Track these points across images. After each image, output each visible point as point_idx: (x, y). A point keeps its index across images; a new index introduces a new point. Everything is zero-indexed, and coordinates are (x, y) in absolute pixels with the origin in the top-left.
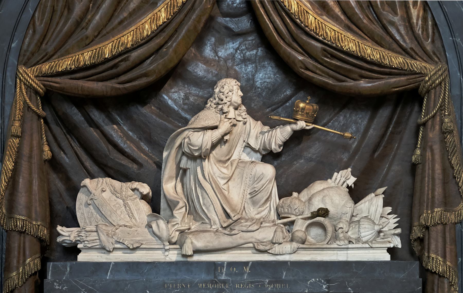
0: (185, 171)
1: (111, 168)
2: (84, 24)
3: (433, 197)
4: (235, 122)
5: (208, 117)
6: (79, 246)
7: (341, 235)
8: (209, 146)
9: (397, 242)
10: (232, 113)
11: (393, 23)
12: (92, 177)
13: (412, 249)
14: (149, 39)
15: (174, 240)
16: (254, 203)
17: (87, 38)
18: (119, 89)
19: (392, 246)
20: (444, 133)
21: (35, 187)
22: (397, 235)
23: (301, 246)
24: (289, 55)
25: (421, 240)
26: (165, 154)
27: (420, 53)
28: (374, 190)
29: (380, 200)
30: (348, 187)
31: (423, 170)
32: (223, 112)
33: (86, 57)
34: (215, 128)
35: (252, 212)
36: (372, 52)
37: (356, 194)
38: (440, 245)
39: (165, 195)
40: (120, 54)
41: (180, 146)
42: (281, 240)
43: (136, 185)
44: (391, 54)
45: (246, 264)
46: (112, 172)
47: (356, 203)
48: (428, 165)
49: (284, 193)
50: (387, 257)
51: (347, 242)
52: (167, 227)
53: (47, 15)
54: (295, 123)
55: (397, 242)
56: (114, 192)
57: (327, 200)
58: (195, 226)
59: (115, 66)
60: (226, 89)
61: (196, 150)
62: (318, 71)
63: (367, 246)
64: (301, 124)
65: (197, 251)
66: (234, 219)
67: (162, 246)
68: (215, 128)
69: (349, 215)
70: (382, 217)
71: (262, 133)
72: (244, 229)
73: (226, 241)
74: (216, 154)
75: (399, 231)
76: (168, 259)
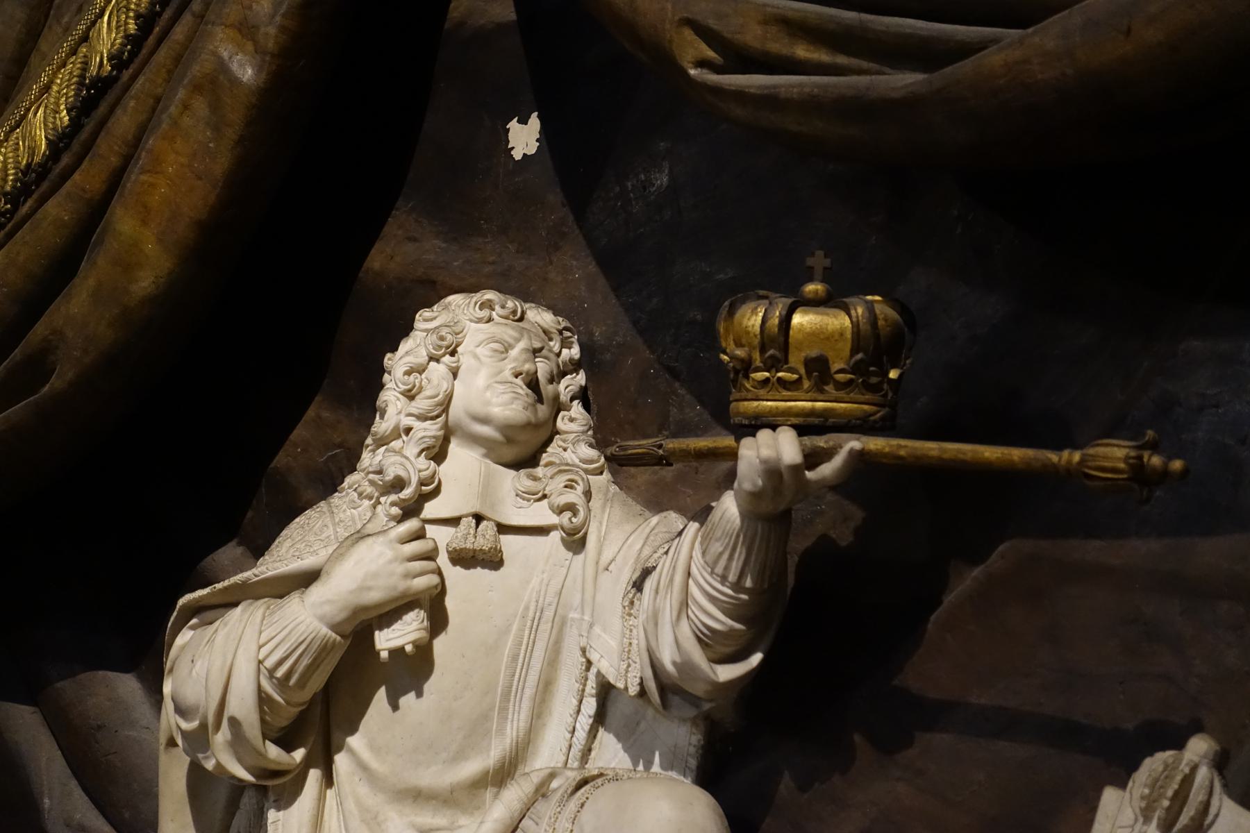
62: (802, 52)
74: (373, 747)
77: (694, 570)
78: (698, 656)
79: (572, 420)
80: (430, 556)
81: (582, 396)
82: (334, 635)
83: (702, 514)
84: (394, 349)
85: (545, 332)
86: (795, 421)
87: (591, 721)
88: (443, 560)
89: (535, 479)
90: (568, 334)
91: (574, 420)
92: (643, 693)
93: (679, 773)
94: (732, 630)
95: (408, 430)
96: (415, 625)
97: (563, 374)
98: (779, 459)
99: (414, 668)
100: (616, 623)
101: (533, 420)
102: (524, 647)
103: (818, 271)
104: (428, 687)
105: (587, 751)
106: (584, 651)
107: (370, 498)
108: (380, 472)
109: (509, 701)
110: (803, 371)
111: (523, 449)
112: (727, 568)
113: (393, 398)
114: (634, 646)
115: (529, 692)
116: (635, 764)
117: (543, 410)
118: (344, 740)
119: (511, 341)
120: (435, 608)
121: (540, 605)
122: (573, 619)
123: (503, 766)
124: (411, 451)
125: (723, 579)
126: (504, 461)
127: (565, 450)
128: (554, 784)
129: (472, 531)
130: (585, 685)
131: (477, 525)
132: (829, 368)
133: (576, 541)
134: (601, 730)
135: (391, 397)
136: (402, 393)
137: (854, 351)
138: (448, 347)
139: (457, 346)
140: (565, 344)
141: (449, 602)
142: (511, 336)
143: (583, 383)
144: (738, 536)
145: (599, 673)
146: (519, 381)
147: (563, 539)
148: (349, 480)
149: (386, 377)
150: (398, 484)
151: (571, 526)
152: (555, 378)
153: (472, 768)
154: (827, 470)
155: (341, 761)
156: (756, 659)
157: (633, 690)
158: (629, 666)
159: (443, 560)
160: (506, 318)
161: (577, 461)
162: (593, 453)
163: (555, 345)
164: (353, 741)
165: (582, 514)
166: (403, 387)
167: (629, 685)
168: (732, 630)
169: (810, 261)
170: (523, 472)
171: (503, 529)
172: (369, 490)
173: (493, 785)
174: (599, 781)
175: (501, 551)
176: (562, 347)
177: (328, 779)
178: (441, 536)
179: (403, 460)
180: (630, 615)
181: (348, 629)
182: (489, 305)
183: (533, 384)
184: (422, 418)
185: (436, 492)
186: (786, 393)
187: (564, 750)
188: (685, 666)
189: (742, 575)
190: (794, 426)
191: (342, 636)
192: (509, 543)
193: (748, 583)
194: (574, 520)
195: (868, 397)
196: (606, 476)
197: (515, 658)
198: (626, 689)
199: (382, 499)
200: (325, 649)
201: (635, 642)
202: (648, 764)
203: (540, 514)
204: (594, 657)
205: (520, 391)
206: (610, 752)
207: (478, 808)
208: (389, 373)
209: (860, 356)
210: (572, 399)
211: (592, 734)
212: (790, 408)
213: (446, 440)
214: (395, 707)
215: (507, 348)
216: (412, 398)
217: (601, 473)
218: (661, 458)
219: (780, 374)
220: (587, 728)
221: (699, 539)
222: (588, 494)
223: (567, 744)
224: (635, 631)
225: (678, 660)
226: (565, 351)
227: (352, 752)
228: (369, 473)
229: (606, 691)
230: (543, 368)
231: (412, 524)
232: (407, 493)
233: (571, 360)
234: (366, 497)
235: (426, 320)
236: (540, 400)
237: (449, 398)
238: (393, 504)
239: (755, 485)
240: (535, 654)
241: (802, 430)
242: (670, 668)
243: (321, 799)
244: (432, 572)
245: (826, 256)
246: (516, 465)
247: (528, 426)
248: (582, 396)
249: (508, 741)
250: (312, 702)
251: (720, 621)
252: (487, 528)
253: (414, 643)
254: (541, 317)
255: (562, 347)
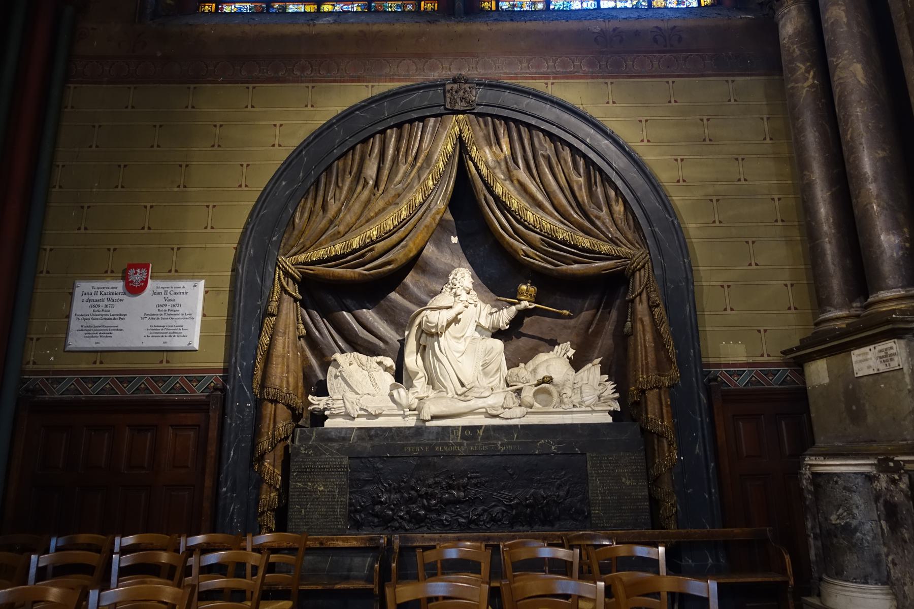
0: (425, 347)
1: (361, 346)
2: (336, 222)
3: (647, 364)
4: (467, 304)
5: (444, 299)
6: (326, 413)
7: (566, 400)
8: (445, 324)
9: (616, 406)
10: (464, 296)
11: (598, 218)
12: (343, 352)
13: (629, 410)
14: (391, 233)
15: (414, 407)
16: (486, 375)
17: (339, 233)
18: (366, 275)
19: (612, 409)
20: (651, 307)
21: (390, 267)
22: (615, 399)
23: (530, 410)
24: (511, 246)
25: (637, 404)
26: (407, 333)
27: (625, 241)
28: (590, 361)
29: (598, 369)
30: (568, 357)
31: (636, 340)
32: (456, 295)
33: (337, 248)
34: (451, 307)
35: (485, 382)
36: (585, 242)
37: (577, 363)
38: (657, 407)
39: (406, 369)
40: (366, 246)
41: (420, 324)
42: (511, 405)
43: (380, 358)
44: (599, 242)
45: (479, 427)
46: (358, 348)
47: (577, 370)
48: (640, 335)
49: (512, 363)
50: (609, 419)
51: (571, 406)
52: (407, 394)
53: (306, 215)
54: (519, 303)
55: (616, 406)
56: (361, 365)
57: (551, 368)
58: (432, 394)
59: (363, 255)
60: (459, 276)
61: (433, 327)
63: (589, 409)
64: (525, 304)
65: (434, 418)
66: (469, 387)
67: (402, 412)
68: (451, 307)
69: (571, 382)
70: (600, 384)
71: (491, 314)
72: (478, 395)
73: (461, 406)
75: (617, 395)
76: (408, 425)
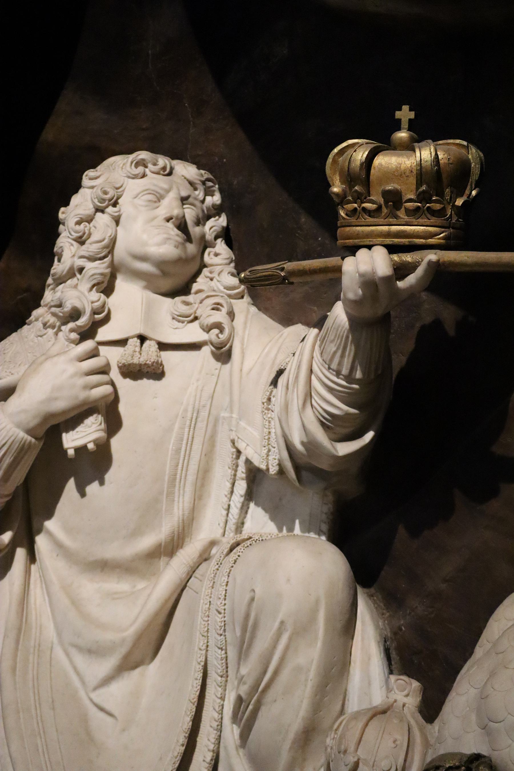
74: (69, 530)
77: (315, 368)
78: (321, 436)
79: (216, 255)
80: (104, 370)
81: (226, 235)
82: (29, 438)
83: (319, 324)
84: (66, 203)
85: (191, 183)
86: (388, 241)
87: (242, 499)
88: (115, 374)
89: (187, 304)
90: (210, 184)
91: (220, 254)
92: (281, 472)
93: (316, 534)
94: (347, 414)
95: (81, 270)
96: (95, 427)
97: (208, 217)
98: (374, 273)
99: (96, 463)
100: (258, 417)
101: (183, 256)
102: (185, 442)
103: (405, 124)
104: (108, 477)
105: (240, 526)
106: (233, 442)
107: (53, 327)
108: (60, 306)
109: (174, 486)
110: (382, 201)
111: (177, 281)
112: (340, 364)
113: (67, 245)
114: (273, 434)
115: (191, 478)
116: (280, 530)
117: (192, 248)
118: (42, 525)
119: (162, 192)
120: (110, 413)
121: (196, 407)
122: (224, 418)
123: (173, 539)
124: (85, 286)
125: (338, 374)
126: (163, 290)
127: (212, 279)
128: (214, 551)
129: (138, 349)
130: (236, 471)
131: (142, 343)
132: (402, 199)
133: (223, 354)
134: (252, 505)
135: (65, 243)
136: (75, 240)
137: (419, 184)
138: (110, 200)
139: (118, 198)
140: (208, 192)
141: (122, 408)
142: (162, 189)
143: (225, 224)
144: (347, 337)
145: (248, 462)
146: (170, 225)
147: (213, 353)
148: (36, 313)
149: (61, 227)
150: (75, 314)
151: (218, 341)
152: (200, 222)
153: (147, 542)
154: (411, 279)
155: (41, 542)
156: (369, 436)
157: (273, 470)
158: (269, 451)
159: (115, 374)
160: (158, 173)
161: (222, 288)
162: (235, 281)
163: (200, 194)
164: (49, 524)
165: (227, 331)
166: (75, 235)
167: (270, 467)
168: (348, 414)
169: (398, 114)
170: (178, 299)
171: (163, 346)
172: (52, 320)
173: (165, 555)
174: (249, 542)
175: (161, 364)
176: (206, 194)
177: (32, 557)
178: (113, 356)
179: (77, 294)
180: (268, 409)
181: (41, 432)
182: (142, 163)
183: (182, 226)
184: (92, 259)
185: (107, 319)
186: (370, 220)
187: (222, 524)
188: (311, 445)
189: (352, 369)
190: (387, 246)
191: (36, 439)
192: (169, 358)
193: (358, 375)
194: (220, 335)
195: (433, 220)
196: (247, 299)
197: (178, 451)
198: (268, 469)
199: (63, 328)
200: (23, 450)
201: (273, 431)
202: (291, 529)
203: (192, 333)
204: (241, 446)
205: (172, 233)
206: (258, 521)
207: (154, 574)
208: (64, 224)
209: (424, 188)
210: (216, 238)
211: (244, 509)
212: (372, 231)
213: (113, 277)
214: (83, 494)
215: (159, 198)
216: (82, 243)
217: (242, 297)
218: (284, 278)
219: (364, 205)
220: (239, 505)
221: (318, 343)
222: (231, 315)
223: (224, 520)
224: (272, 423)
225: (305, 440)
226: (209, 199)
227: (50, 534)
228: (51, 307)
229: (255, 475)
230: (190, 214)
231: (88, 345)
232: (83, 321)
233: (214, 206)
234: (49, 327)
235: (91, 179)
236: (189, 238)
237: (113, 241)
238: (72, 330)
239: (356, 294)
240: (195, 447)
241: (392, 249)
242: (299, 447)
243: (28, 572)
244: (107, 383)
245: (400, 110)
246: (172, 294)
247: (180, 261)
248: (226, 235)
249: (176, 519)
250: (15, 495)
251: (340, 408)
252: (150, 347)
253: (95, 441)
254: (186, 170)
255: (206, 194)
